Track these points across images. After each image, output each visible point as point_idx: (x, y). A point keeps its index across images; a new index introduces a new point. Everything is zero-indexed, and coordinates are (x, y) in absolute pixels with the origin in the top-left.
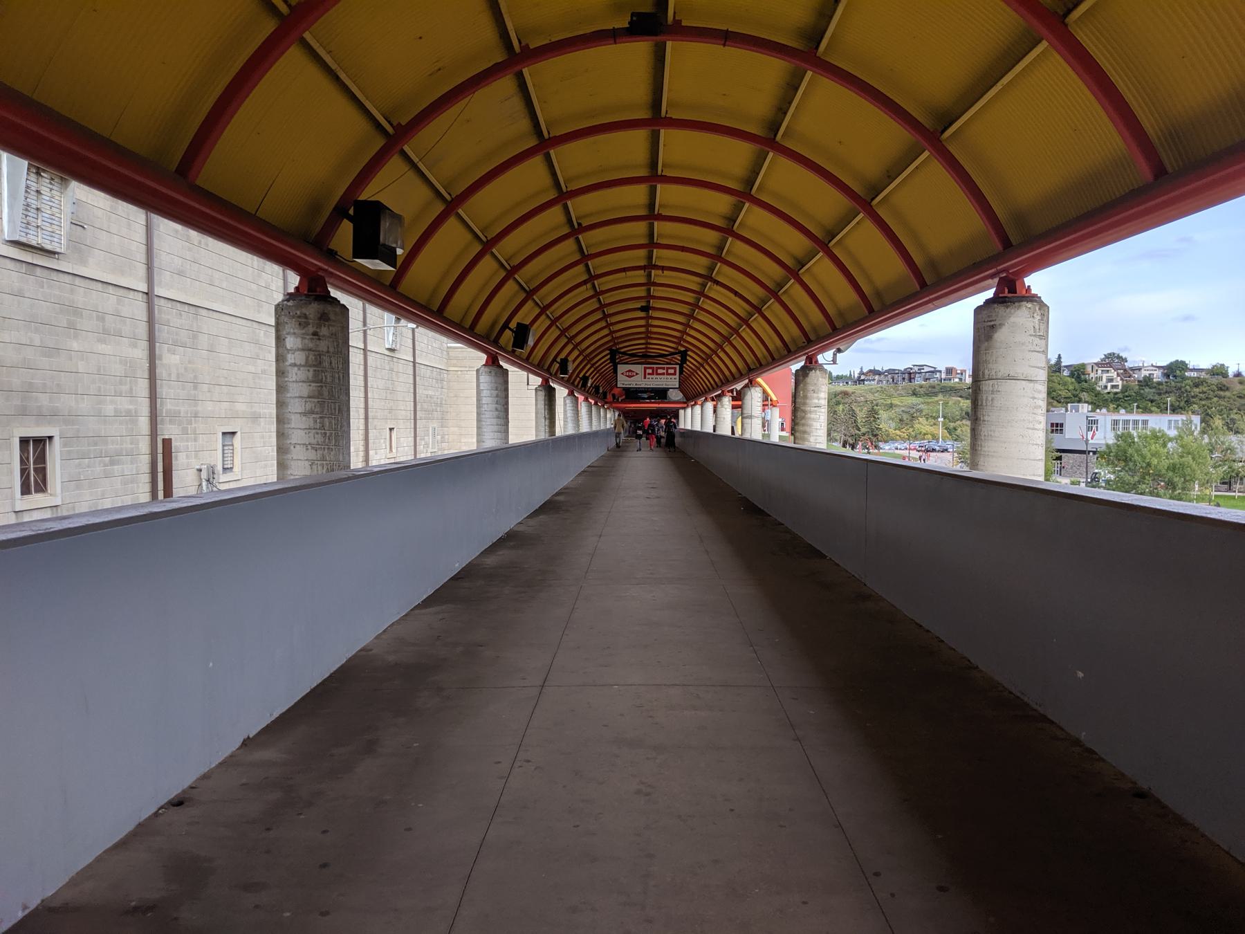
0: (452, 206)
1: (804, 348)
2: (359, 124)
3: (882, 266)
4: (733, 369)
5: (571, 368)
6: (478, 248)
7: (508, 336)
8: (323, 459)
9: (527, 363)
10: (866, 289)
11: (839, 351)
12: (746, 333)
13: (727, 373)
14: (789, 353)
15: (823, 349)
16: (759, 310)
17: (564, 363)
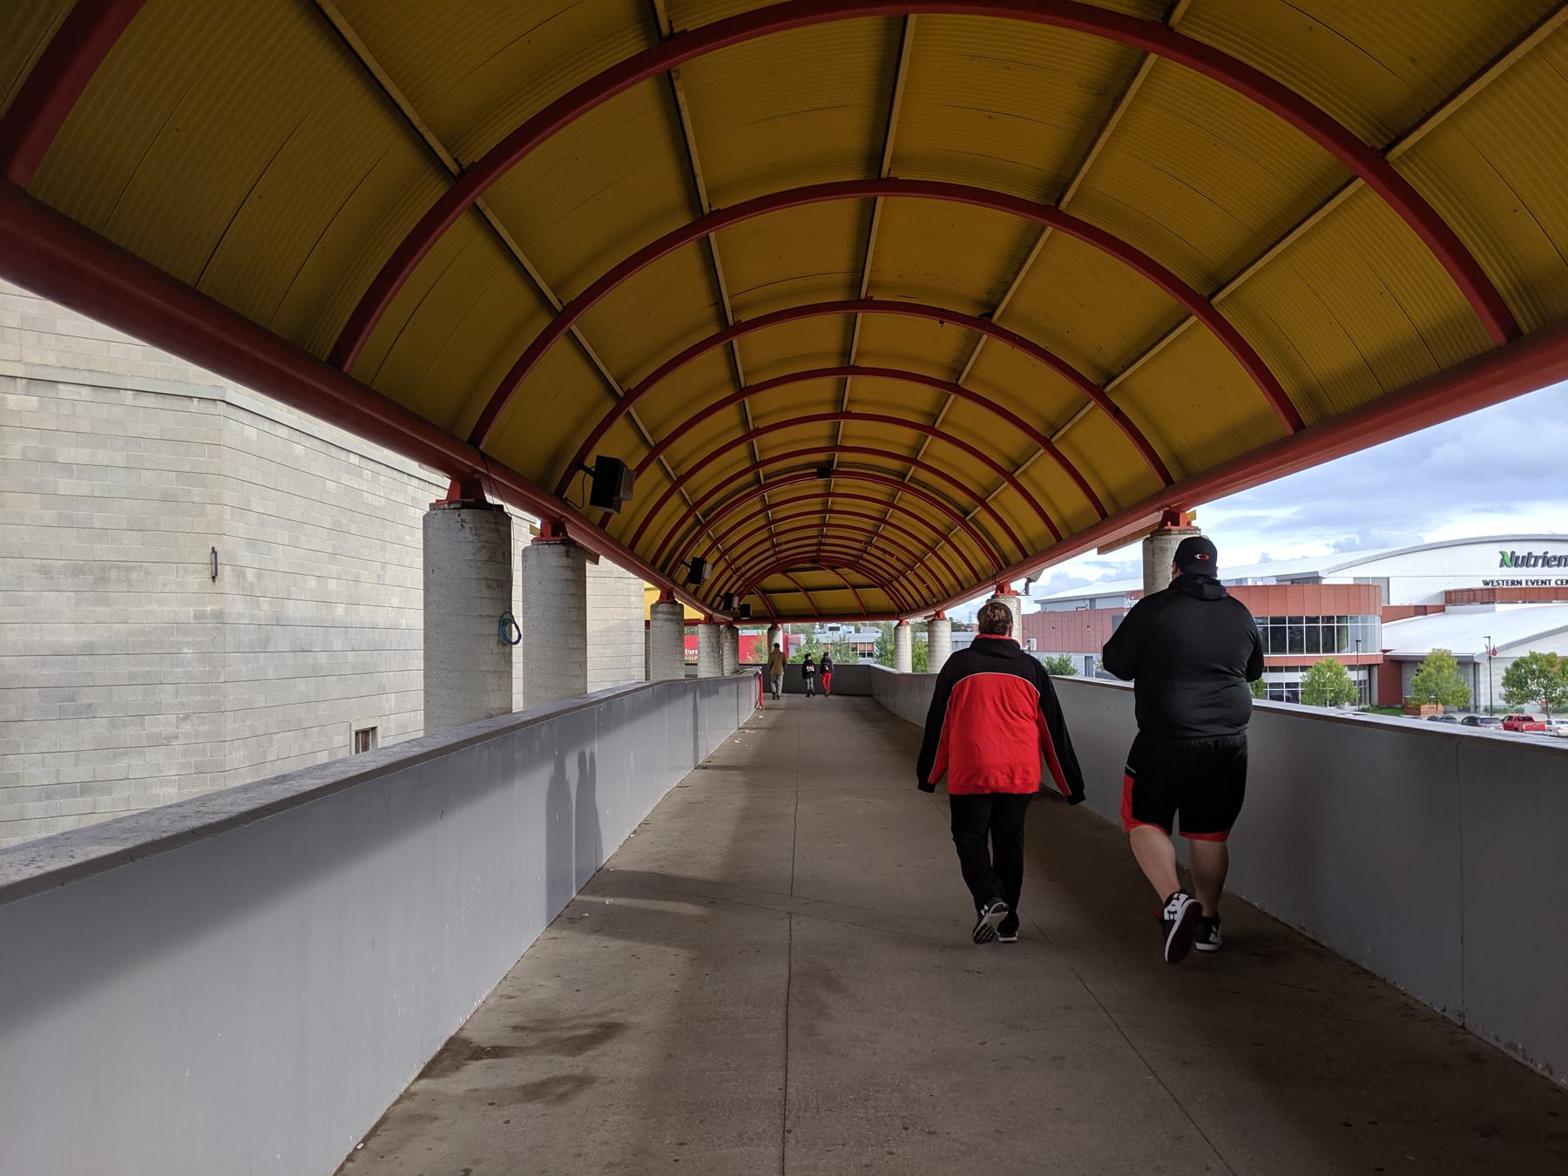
0: (656, 451)
1: (994, 577)
2: (593, 387)
3: (1068, 501)
4: (925, 593)
5: (708, 574)
6: (435, 191)
7: (581, 486)
8: (808, 663)
9: (631, 555)
10: (1054, 519)
11: (1030, 580)
12: (946, 551)
13: (917, 596)
14: (927, 606)
15: (1015, 577)
16: (932, 550)
17: (698, 564)
